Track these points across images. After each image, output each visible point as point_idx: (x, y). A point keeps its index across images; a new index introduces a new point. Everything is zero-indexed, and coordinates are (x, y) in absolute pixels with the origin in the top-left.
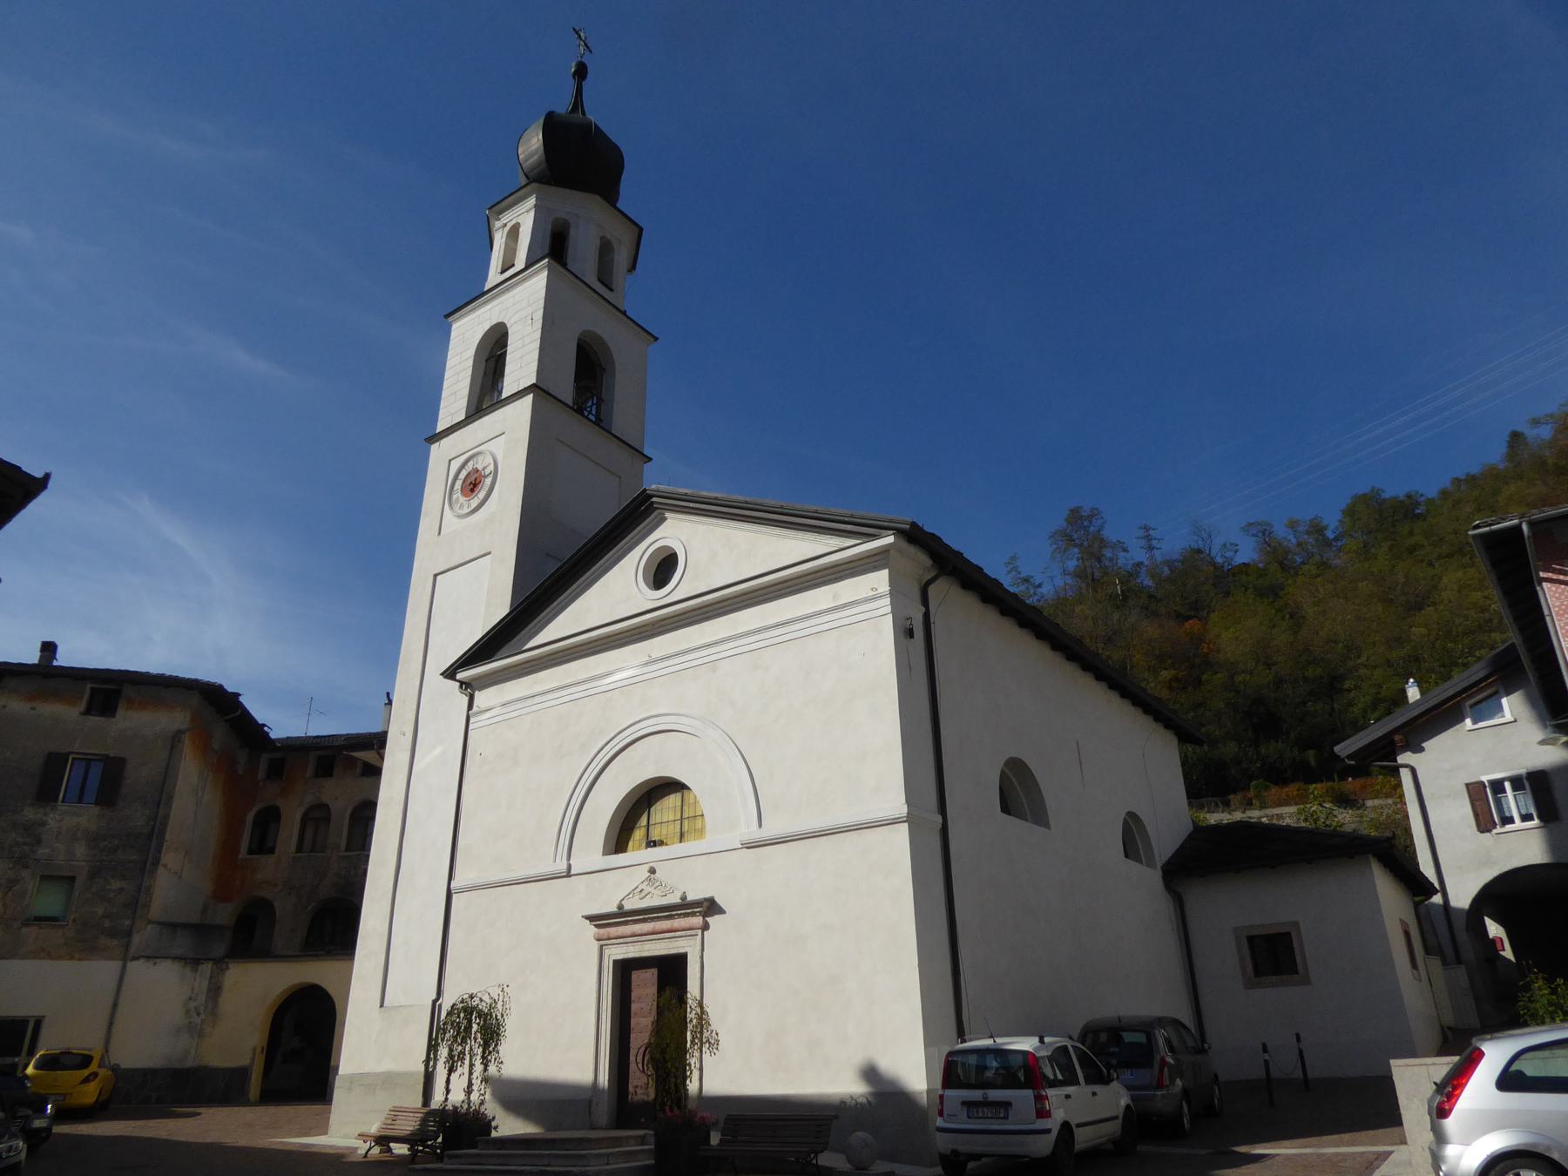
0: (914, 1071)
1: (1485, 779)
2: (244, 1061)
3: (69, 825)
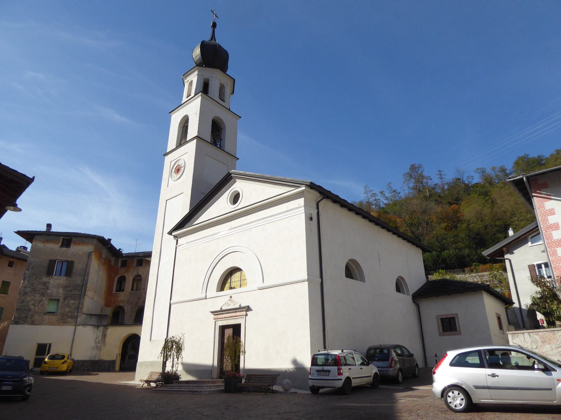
0: (307, 363)
1: (535, 263)
2: (114, 358)
3: (57, 282)
